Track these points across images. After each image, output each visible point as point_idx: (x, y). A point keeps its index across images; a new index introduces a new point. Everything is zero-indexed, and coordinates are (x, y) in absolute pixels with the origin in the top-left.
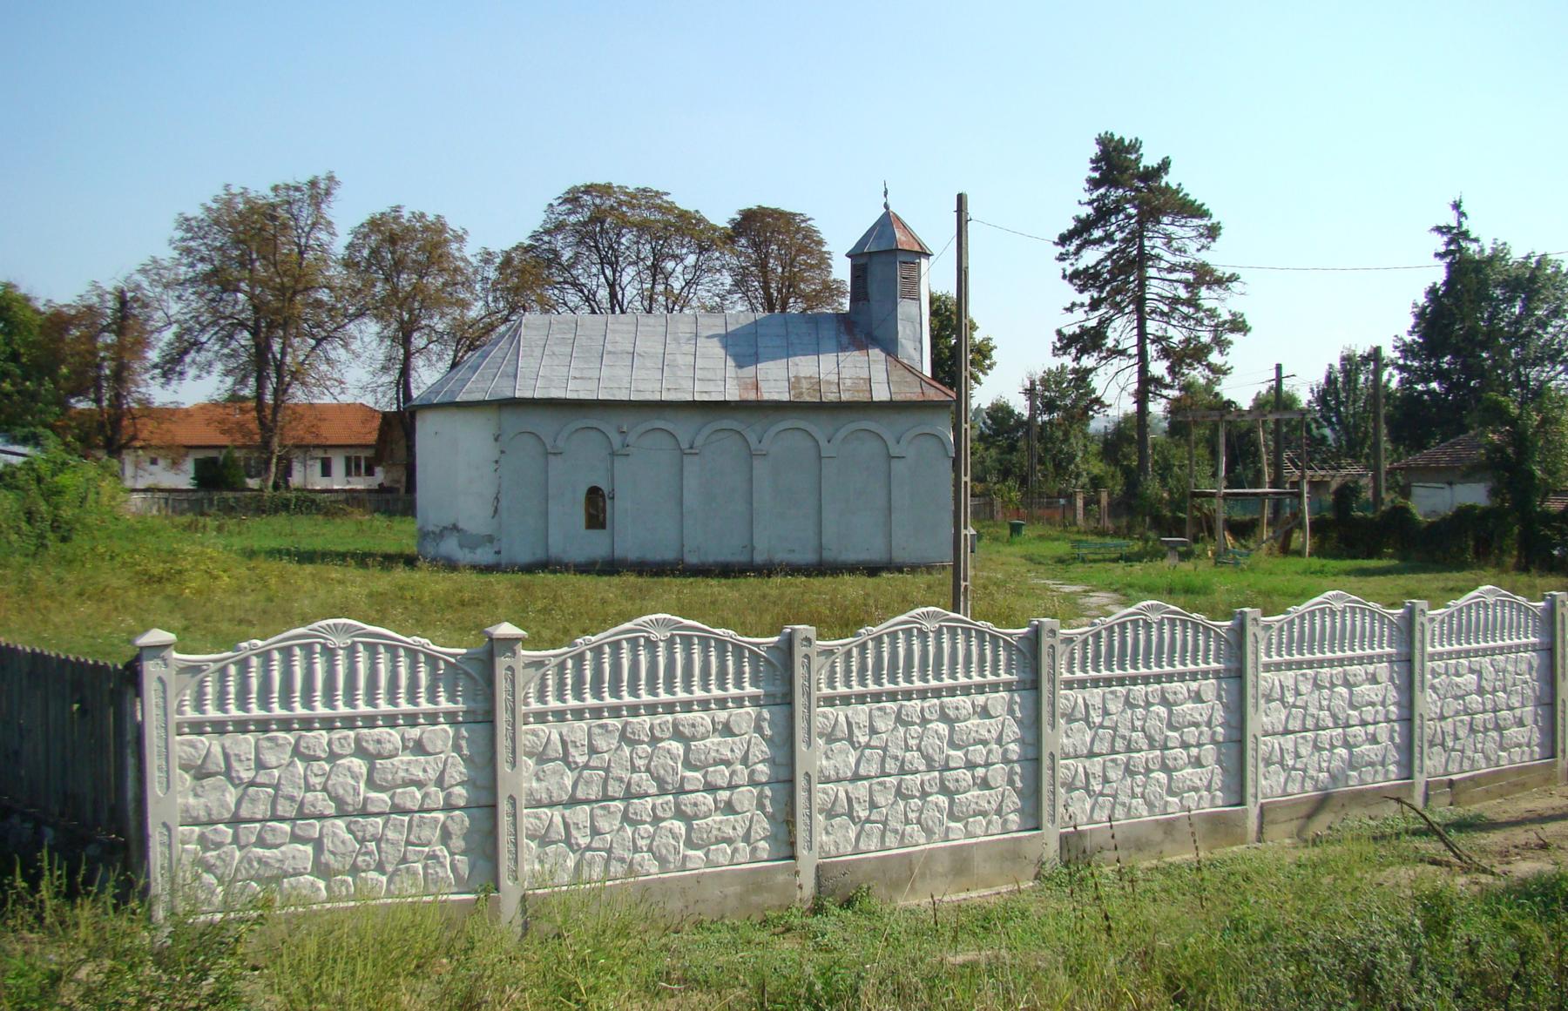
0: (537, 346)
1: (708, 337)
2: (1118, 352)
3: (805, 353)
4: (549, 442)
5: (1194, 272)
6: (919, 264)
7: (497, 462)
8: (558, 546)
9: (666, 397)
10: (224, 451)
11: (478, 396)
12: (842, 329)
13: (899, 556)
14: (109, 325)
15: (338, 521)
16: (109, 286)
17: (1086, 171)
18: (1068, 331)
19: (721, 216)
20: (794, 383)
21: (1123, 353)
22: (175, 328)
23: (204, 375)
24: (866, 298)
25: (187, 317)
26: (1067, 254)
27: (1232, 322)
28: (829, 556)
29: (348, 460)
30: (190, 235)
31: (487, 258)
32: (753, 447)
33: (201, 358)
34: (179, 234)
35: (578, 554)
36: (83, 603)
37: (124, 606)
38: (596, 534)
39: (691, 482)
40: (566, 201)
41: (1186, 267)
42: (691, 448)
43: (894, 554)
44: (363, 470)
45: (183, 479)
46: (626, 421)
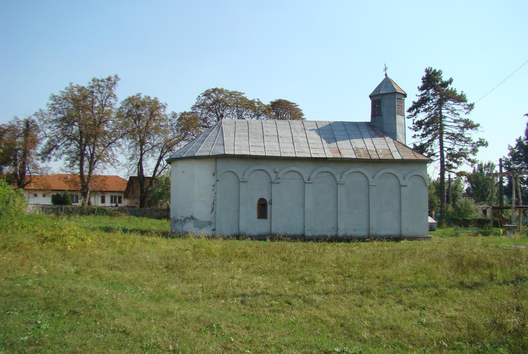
0: (231, 132)
1: (310, 130)
4: (240, 177)
6: (404, 100)
7: (214, 186)
9: (298, 155)
10: (63, 192)
11: (207, 154)
12: (370, 128)
13: (405, 233)
14: (21, 134)
15: (116, 218)
16: (22, 118)
19: (266, 102)
20: (356, 150)
22: (48, 139)
23: (58, 159)
24: (380, 115)
25: (53, 135)
27: (480, 142)
28: (373, 232)
29: (112, 197)
30: (55, 102)
31: (174, 115)
32: (338, 180)
33: (58, 152)
34: (51, 102)
35: (255, 232)
36: (6, 253)
37: (32, 255)
38: (262, 221)
39: (309, 197)
40: (205, 95)
41: (460, 120)
42: (309, 180)
43: (402, 233)
45: (48, 201)
46: (277, 166)
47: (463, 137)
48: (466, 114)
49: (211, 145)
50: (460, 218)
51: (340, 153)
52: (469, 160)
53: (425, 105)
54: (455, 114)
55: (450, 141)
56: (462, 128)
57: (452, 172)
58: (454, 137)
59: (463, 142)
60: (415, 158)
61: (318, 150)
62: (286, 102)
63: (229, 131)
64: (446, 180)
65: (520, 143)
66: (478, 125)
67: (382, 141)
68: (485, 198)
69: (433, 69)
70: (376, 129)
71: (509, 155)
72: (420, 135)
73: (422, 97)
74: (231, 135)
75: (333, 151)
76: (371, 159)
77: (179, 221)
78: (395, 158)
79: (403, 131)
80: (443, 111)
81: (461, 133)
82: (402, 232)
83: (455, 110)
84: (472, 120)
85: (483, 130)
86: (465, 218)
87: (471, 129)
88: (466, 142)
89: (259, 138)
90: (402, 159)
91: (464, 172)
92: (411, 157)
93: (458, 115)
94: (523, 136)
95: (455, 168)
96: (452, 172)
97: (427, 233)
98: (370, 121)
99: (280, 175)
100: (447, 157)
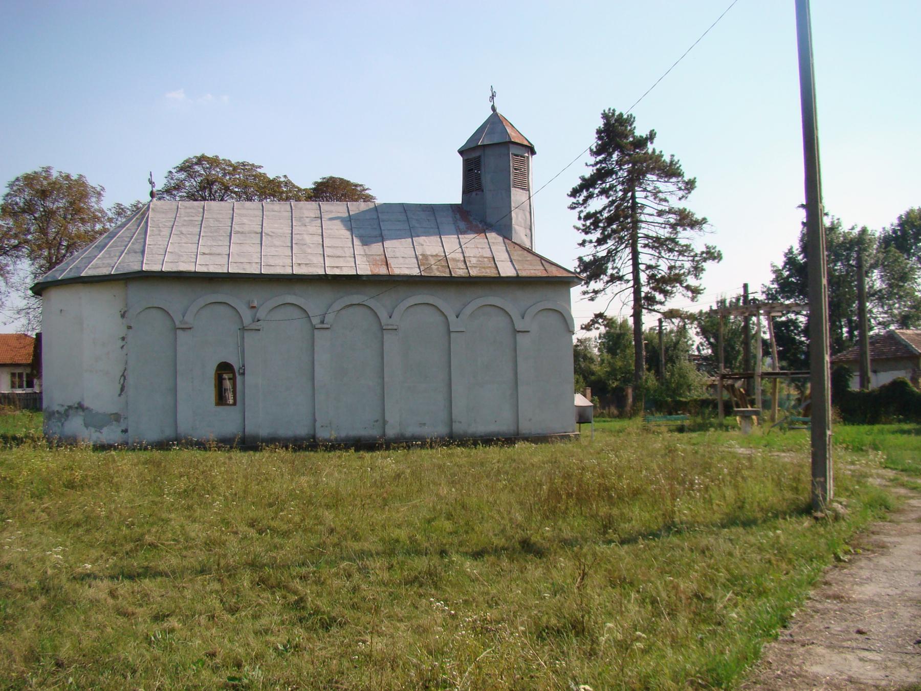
0: (165, 226)
1: (331, 219)
2: (614, 279)
3: (427, 234)
4: (177, 319)
5: (680, 215)
6: (528, 158)
7: (123, 339)
8: (187, 424)
9: (297, 271)
11: (104, 271)
12: (458, 216)
13: (526, 427)
17: (592, 141)
18: (587, 259)
19: (306, 182)
20: (422, 260)
21: (620, 278)
24: (480, 189)
26: (578, 204)
27: (707, 253)
28: (458, 428)
32: (383, 323)
35: (209, 432)
39: (322, 358)
41: (671, 211)
42: (322, 322)
44: (25, 383)
46: (256, 295)
47: (677, 243)
48: (680, 199)
49: (118, 254)
50: (669, 399)
51: (387, 265)
52: (688, 288)
53: (604, 182)
54: (661, 200)
55: (650, 251)
56: (673, 226)
57: (654, 310)
58: (658, 243)
59: (676, 254)
60: (544, 274)
61: (341, 259)
62: (342, 181)
63: (160, 225)
64: (858, 373)
65: (790, 261)
66: (704, 221)
67: (481, 240)
68: (731, 364)
69: (617, 113)
70: (471, 218)
71: (773, 282)
72: (594, 241)
73: (598, 166)
74: (162, 234)
75: (375, 264)
76: (451, 277)
77: (57, 415)
78: (502, 275)
79: (525, 221)
80: (637, 194)
81: (672, 236)
82: (520, 428)
83: (660, 192)
84: (693, 210)
85: (714, 229)
86: (678, 398)
87: (692, 228)
88: (681, 253)
89: (221, 238)
90: (518, 276)
91: (677, 311)
92: (536, 272)
93: (666, 200)
94: (797, 248)
95: (662, 303)
96: (654, 310)
97: (573, 429)
98: (460, 202)
99: (261, 314)
100: (649, 283)
